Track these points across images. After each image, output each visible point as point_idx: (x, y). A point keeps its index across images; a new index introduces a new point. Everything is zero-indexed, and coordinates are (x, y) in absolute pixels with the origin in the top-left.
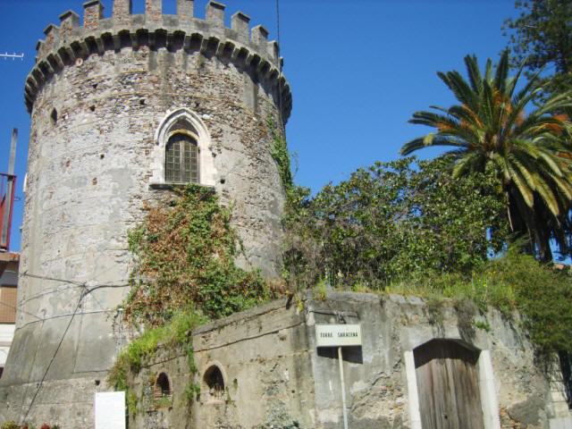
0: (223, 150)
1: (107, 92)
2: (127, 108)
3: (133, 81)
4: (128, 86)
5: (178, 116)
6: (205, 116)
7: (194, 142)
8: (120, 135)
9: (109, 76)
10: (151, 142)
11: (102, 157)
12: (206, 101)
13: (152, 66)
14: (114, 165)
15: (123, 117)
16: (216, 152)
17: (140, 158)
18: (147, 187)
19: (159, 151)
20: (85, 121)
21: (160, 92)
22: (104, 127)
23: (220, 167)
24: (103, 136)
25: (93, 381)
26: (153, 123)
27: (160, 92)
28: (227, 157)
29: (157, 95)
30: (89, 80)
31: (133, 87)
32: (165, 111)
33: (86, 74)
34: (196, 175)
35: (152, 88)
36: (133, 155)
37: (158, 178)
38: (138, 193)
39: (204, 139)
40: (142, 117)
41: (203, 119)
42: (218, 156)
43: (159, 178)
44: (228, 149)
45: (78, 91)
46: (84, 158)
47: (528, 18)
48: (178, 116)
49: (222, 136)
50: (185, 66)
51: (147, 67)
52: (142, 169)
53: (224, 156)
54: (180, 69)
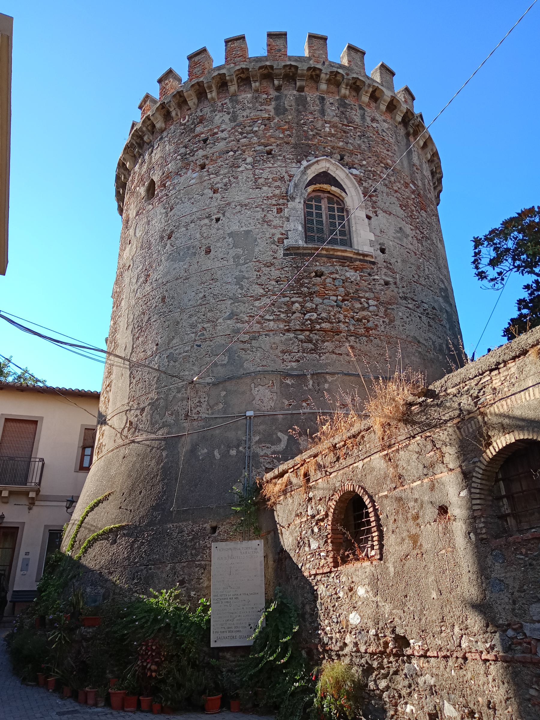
0: (379, 212)
1: (221, 145)
2: (249, 160)
3: (256, 129)
4: (250, 136)
5: (319, 194)
6: (354, 171)
7: (340, 201)
8: (239, 193)
9: (223, 127)
10: (287, 197)
11: (218, 220)
12: (351, 153)
13: (280, 110)
14: (235, 228)
15: (244, 171)
16: (371, 214)
17: (270, 217)
18: (281, 252)
19: (297, 206)
20: (193, 181)
21: (292, 140)
22: (219, 185)
23: (378, 232)
24: (218, 195)
25: (208, 526)
26: (287, 178)
27: (292, 140)
28: (385, 221)
29: (288, 143)
30: (197, 136)
31: (256, 136)
32: (300, 162)
33: (193, 130)
34: (348, 242)
35: (281, 136)
36: (259, 215)
37: (296, 241)
38: (269, 259)
39: (353, 198)
40: (269, 170)
41: (351, 174)
42: (374, 218)
43: (296, 238)
44: (385, 212)
45: (183, 150)
46: (193, 225)
47: (507, 428)
48: (319, 194)
49: (377, 196)
50: (323, 112)
51: (272, 113)
52: (274, 231)
53: (382, 219)
54: (317, 114)
